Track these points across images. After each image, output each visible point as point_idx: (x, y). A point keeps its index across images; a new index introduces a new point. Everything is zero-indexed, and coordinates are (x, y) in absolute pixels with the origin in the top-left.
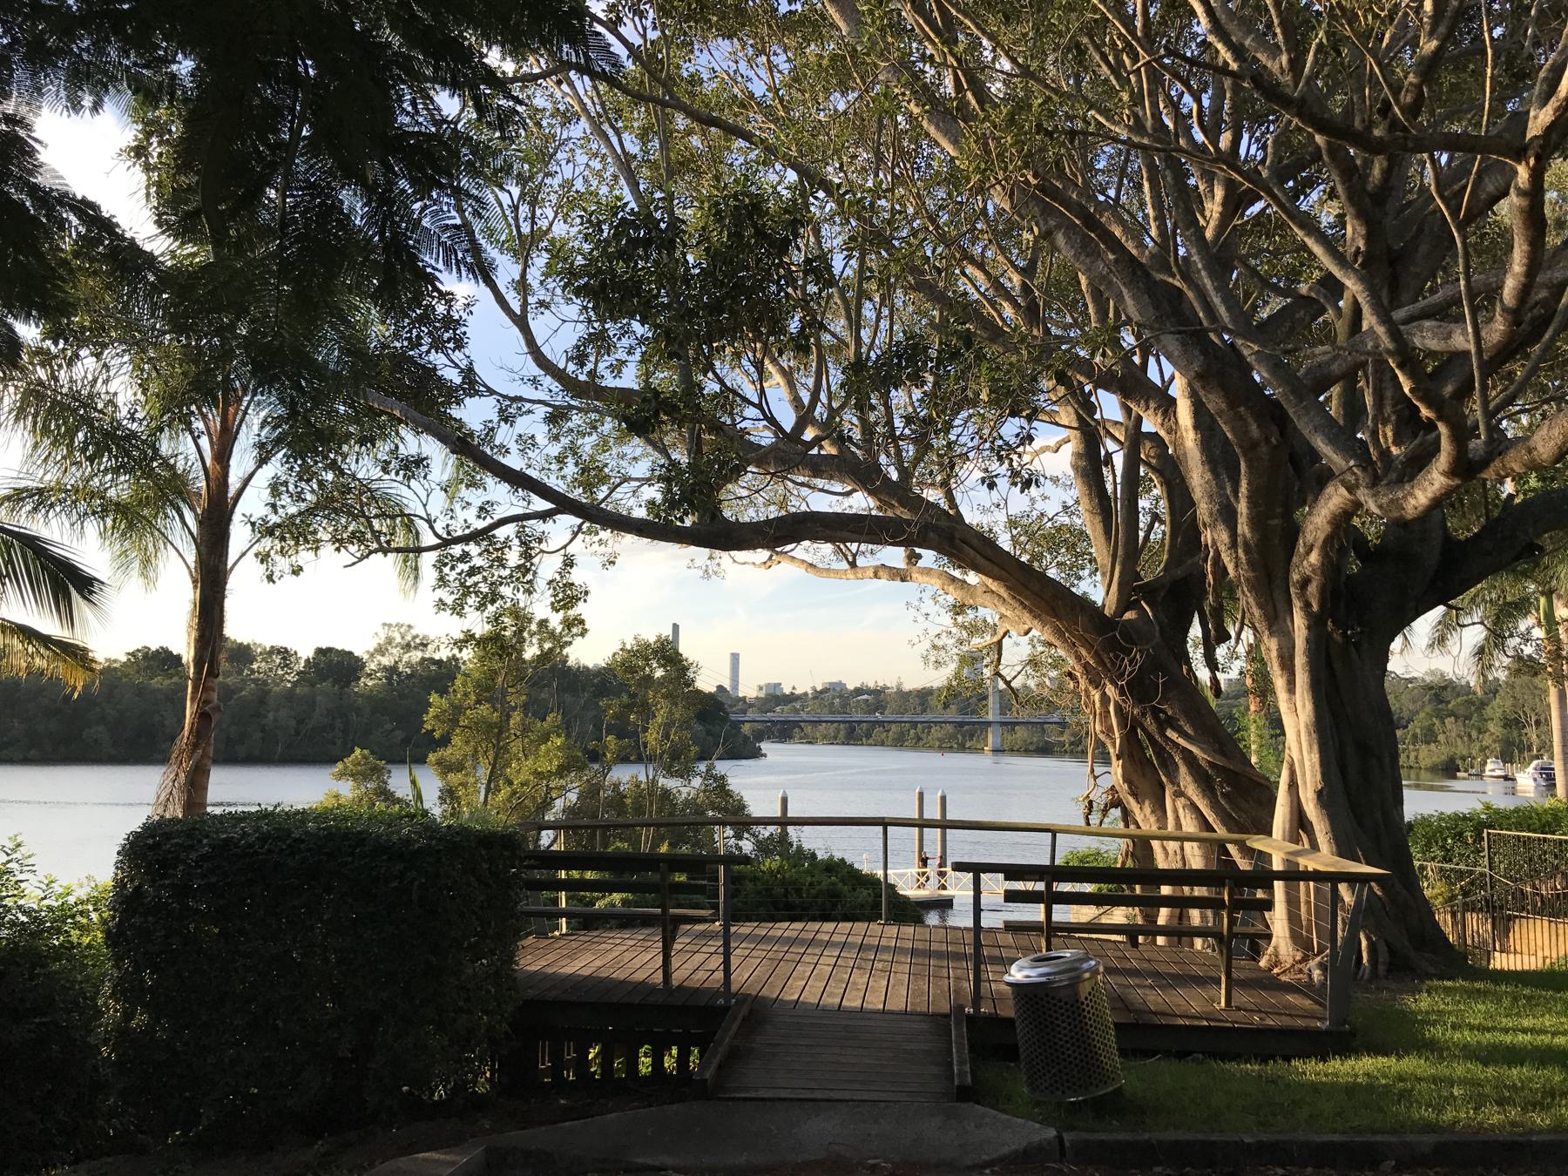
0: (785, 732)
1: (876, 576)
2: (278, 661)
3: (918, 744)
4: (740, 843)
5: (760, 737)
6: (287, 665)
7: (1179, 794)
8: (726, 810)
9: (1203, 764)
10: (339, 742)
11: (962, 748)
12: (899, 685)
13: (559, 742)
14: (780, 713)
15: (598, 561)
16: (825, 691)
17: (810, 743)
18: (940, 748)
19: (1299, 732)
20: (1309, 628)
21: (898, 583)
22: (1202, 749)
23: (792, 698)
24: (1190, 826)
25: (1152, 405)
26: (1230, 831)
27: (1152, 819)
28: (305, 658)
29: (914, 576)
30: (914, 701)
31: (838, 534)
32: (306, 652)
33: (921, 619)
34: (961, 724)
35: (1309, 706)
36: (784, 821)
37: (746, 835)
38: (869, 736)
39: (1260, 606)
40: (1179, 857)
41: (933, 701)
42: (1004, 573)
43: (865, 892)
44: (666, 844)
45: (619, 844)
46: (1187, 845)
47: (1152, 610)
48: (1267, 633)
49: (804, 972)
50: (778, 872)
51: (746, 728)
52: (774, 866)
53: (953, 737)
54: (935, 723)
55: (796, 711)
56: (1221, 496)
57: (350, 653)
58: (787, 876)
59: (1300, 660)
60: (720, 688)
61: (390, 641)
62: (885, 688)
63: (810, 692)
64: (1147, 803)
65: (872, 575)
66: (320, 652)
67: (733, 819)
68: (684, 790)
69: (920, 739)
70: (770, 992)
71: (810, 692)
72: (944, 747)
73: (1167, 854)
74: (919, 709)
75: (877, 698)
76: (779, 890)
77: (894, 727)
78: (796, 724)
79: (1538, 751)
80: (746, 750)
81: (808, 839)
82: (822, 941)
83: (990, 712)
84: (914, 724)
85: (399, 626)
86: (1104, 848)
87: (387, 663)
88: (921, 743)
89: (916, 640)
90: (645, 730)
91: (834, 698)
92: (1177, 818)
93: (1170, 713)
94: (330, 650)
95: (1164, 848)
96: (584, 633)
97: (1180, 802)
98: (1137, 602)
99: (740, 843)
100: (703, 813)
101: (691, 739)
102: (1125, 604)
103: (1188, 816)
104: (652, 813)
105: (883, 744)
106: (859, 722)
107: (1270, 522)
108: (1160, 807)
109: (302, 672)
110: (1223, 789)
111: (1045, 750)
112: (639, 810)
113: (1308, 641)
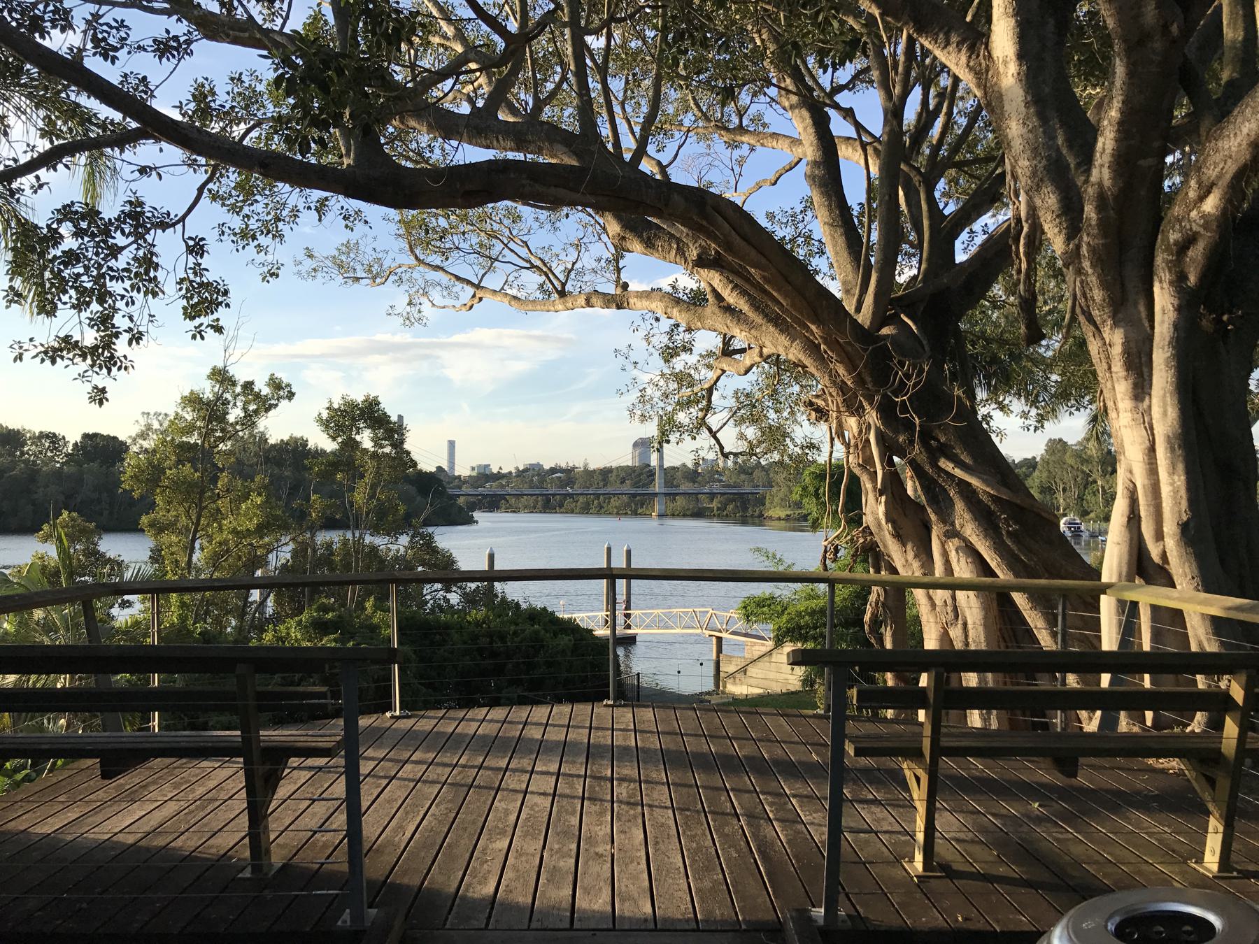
0: (493, 503)
1: (589, 303)
2: (47, 444)
3: (601, 511)
4: (449, 596)
5: (473, 507)
6: (56, 449)
7: (952, 533)
8: (435, 566)
9: (984, 498)
10: (106, 513)
11: (635, 514)
12: (586, 466)
13: (259, 500)
14: (490, 488)
15: (256, 272)
16: (526, 470)
17: (514, 512)
18: (618, 514)
19: (1152, 449)
20: (1179, 309)
21: (612, 312)
22: (984, 481)
23: (499, 476)
24: (963, 570)
25: (954, 39)
26: (1017, 575)
27: (916, 565)
28: (72, 442)
29: (631, 301)
30: (597, 477)
31: (553, 190)
32: (73, 436)
33: (630, 367)
34: (634, 495)
35: (1173, 413)
36: (492, 576)
37: (454, 589)
38: (561, 506)
39: (1104, 285)
40: (949, 609)
41: (612, 477)
42: (764, 261)
43: (567, 638)
44: (372, 599)
45: (324, 600)
46: (960, 594)
47: (915, 323)
48: (1109, 322)
49: (507, 812)
50: (484, 622)
51: (461, 500)
52: (480, 616)
53: (628, 505)
54: (614, 495)
55: (503, 486)
56: (1049, 148)
57: (115, 438)
58: (492, 625)
59: (1161, 356)
60: (440, 468)
61: (149, 427)
62: (574, 468)
63: (514, 471)
64: (909, 546)
65: (583, 302)
66: (86, 436)
67: (441, 574)
68: (393, 547)
69: (601, 507)
70: (444, 880)
71: (514, 471)
72: (620, 513)
73: (933, 605)
74: (601, 484)
75: (568, 475)
76: (484, 641)
77: (581, 499)
78: (503, 497)
79: (1064, 510)
80: (460, 517)
81: (513, 591)
82: (532, 740)
83: (657, 485)
84: (597, 496)
85: (157, 414)
86: (777, 593)
87: (148, 447)
88: (603, 511)
89: (624, 390)
90: (352, 490)
91: (533, 476)
92: (947, 563)
93: (943, 440)
94: (96, 435)
95: (930, 598)
96: (291, 395)
97: (952, 545)
98: (897, 315)
99: (449, 596)
100: (413, 568)
101: (398, 498)
102: (881, 318)
103: (963, 560)
104: (359, 570)
105: (572, 512)
106: (554, 495)
107: (1141, 162)
108: (924, 552)
109: (69, 454)
110: (1008, 527)
111: (698, 514)
112: (347, 567)
113: (1176, 326)
